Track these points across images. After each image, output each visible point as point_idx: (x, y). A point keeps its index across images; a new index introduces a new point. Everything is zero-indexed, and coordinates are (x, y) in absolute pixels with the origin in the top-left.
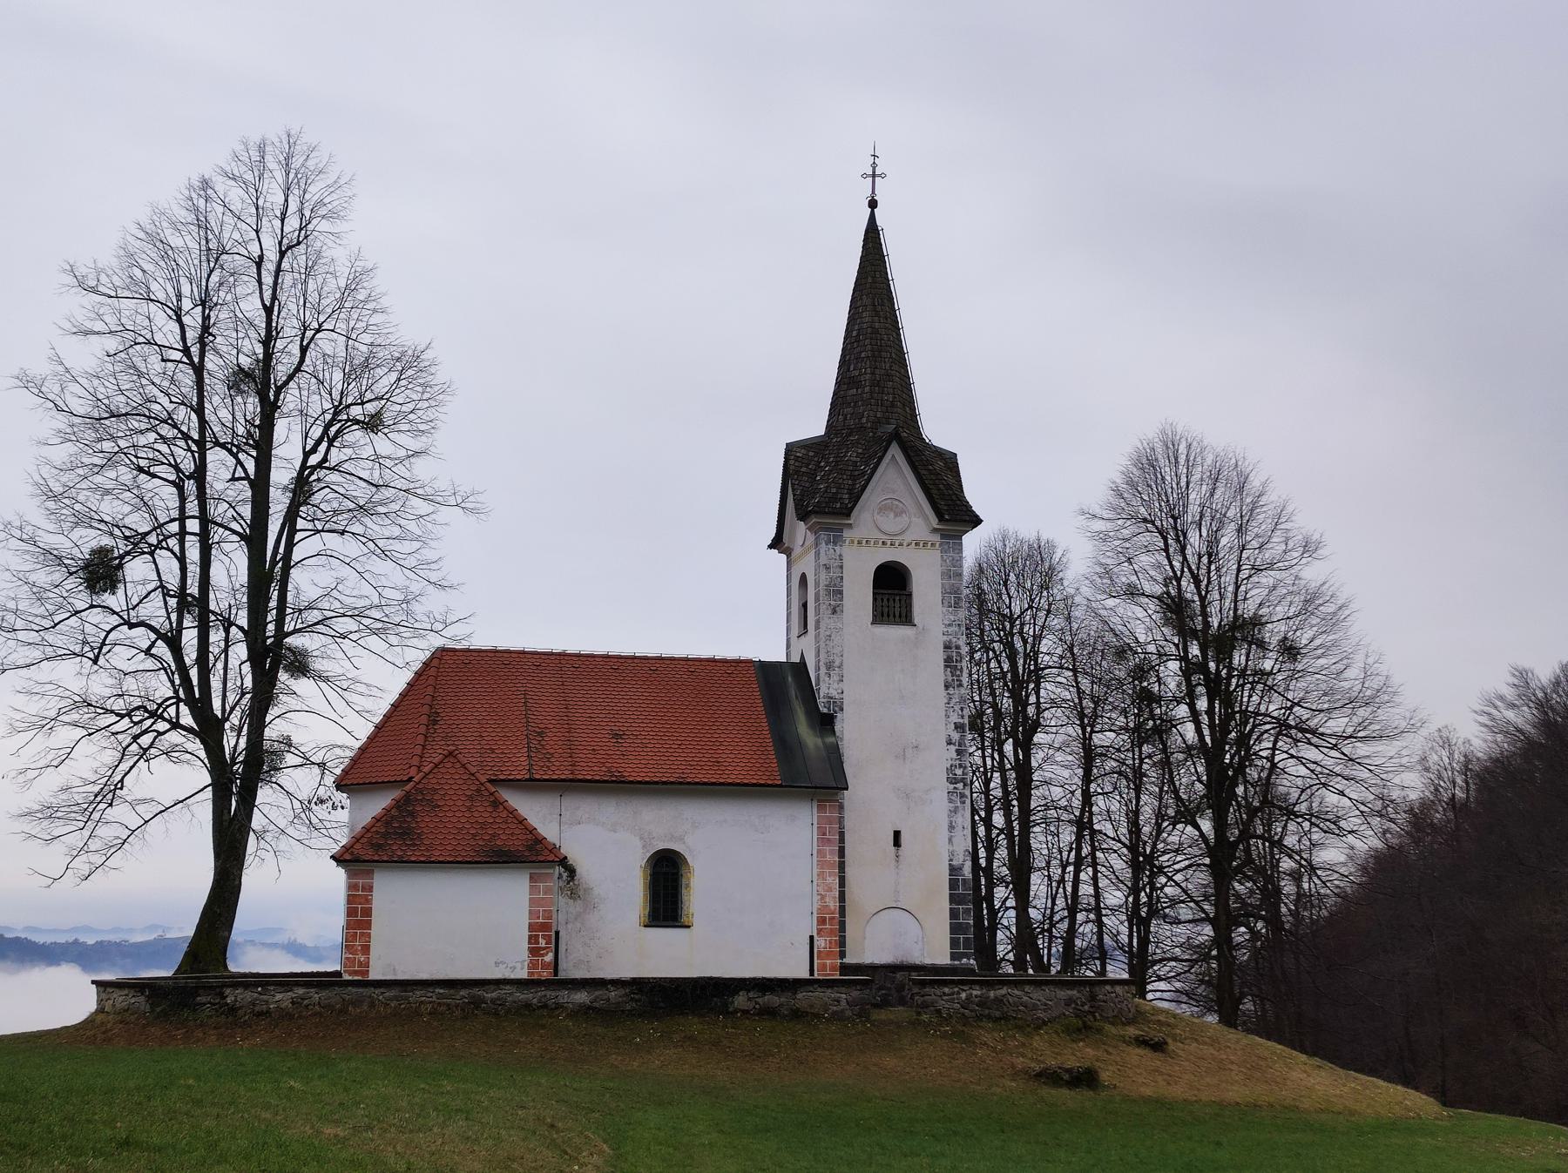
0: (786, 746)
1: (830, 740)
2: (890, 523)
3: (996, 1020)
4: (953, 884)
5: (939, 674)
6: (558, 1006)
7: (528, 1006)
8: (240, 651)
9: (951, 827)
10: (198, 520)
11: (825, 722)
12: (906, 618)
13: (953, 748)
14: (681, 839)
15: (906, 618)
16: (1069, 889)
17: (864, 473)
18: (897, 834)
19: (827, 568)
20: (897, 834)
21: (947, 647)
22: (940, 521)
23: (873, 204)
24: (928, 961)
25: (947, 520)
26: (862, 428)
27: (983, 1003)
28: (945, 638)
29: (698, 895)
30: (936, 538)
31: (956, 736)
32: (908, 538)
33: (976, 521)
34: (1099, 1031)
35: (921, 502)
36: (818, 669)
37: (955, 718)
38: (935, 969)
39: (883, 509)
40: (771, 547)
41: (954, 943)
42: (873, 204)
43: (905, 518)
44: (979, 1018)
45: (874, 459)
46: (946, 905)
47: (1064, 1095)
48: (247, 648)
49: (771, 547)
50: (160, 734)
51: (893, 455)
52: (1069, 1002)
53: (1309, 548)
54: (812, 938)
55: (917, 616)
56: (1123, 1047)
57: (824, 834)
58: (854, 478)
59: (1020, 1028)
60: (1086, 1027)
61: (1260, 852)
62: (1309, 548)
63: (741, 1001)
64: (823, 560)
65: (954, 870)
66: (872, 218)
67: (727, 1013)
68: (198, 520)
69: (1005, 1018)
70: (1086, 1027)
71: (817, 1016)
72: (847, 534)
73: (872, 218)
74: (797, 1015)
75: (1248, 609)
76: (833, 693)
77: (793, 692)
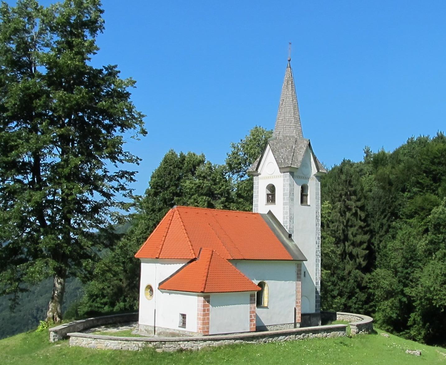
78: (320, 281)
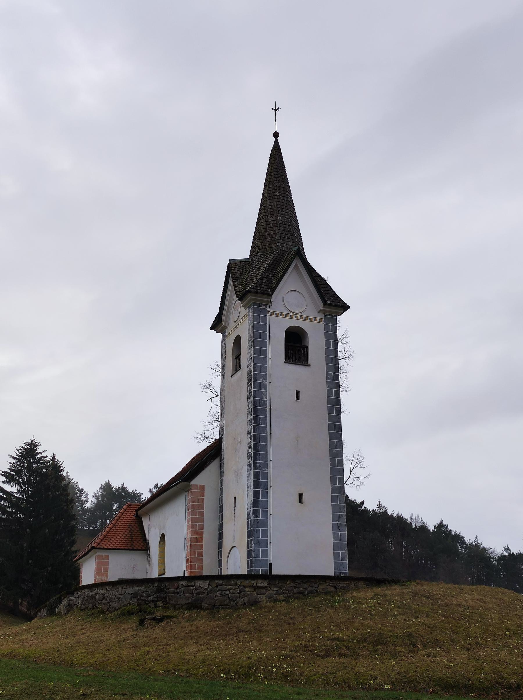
10: (183, 576)
18: (235, 498)
20: (235, 498)
22: (324, 305)
23: (276, 135)
25: (329, 304)
28: (84, 491)
30: (321, 316)
33: (345, 307)
35: (313, 293)
37: (250, 418)
40: (212, 328)
42: (276, 135)
46: (245, 539)
48: (332, 576)
49: (212, 328)
51: (296, 264)
52: (135, 595)
53: (102, 485)
54: (184, 571)
57: (337, 521)
62: (102, 485)
65: (248, 514)
66: (276, 143)
68: (183, 576)
72: (270, 309)
73: (276, 143)
75: (73, 498)
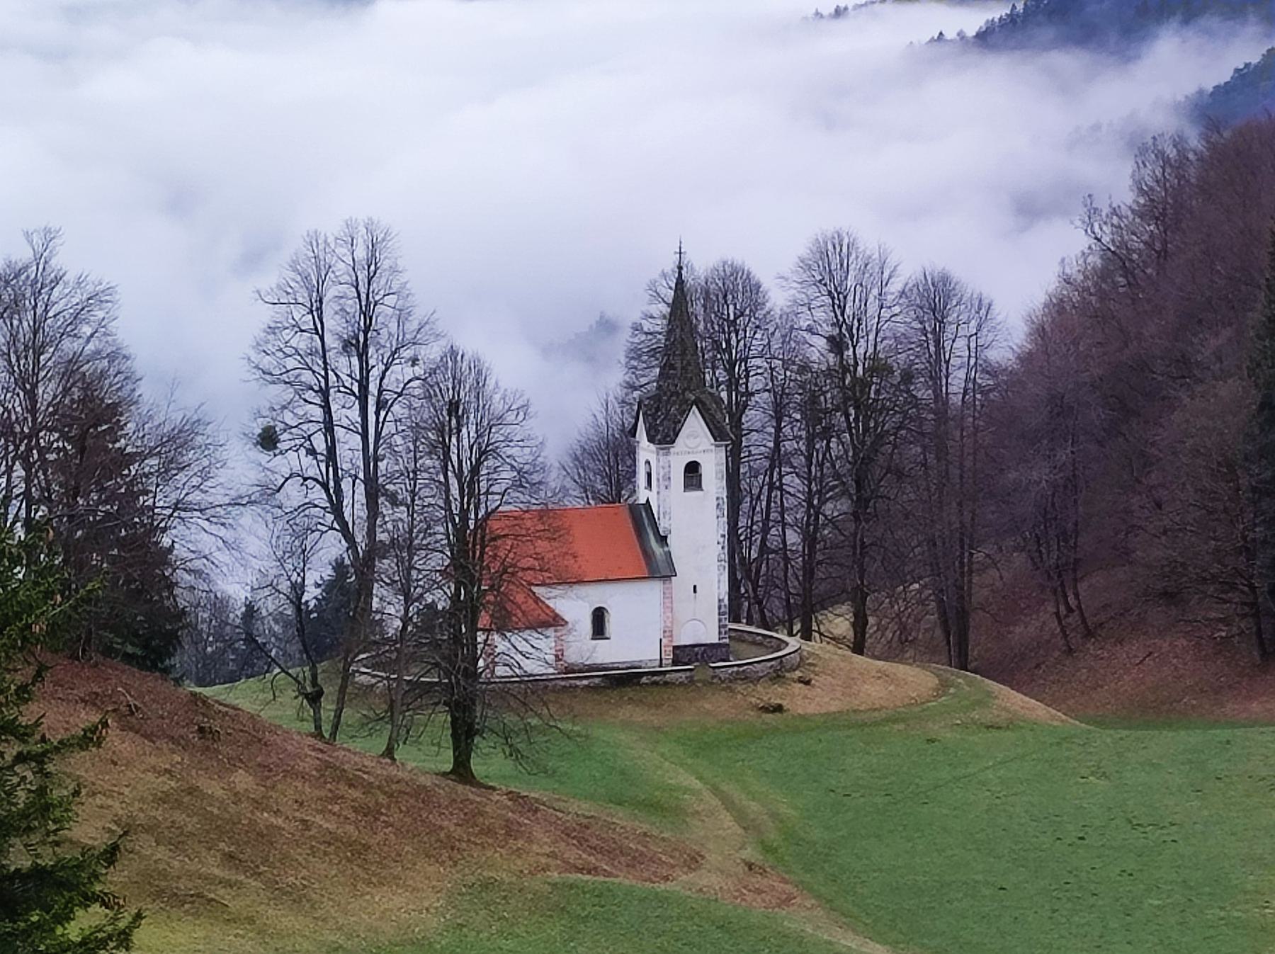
0: (648, 555)
1: (666, 549)
2: (692, 443)
3: (742, 679)
4: (720, 608)
5: (715, 512)
6: (577, 686)
7: (564, 687)
8: (361, 488)
9: (719, 581)
11: (663, 540)
12: (699, 486)
13: (720, 546)
14: (606, 603)
15: (699, 486)
16: (764, 503)
17: (680, 422)
18: (695, 587)
19: (663, 468)
20: (695, 587)
21: (718, 499)
24: (708, 642)
26: (677, 394)
27: (738, 673)
29: (611, 626)
30: (713, 447)
31: (721, 540)
32: (700, 448)
34: (784, 677)
36: (659, 513)
37: (722, 532)
38: (712, 646)
39: (688, 437)
41: (720, 633)
43: (698, 439)
44: (736, 679)
45: (684, 412)
46: (717, 617)
47: (769, 717)
50: (323, 533)
55: (704, 486)
56: (793, 684)
58: (675, 423)
59: (752, 682)
60: (779, 676)
61: (931, 356)
63: (644, 680)
64: (661, 463)
67: (641, 685)
69: (746, 678)
70: (779, 676)
71: (674, 684)
72: (672, 450)
74: (666, 683)
76: (667, 526)
77: (646, 522)
78: (727, 598)
